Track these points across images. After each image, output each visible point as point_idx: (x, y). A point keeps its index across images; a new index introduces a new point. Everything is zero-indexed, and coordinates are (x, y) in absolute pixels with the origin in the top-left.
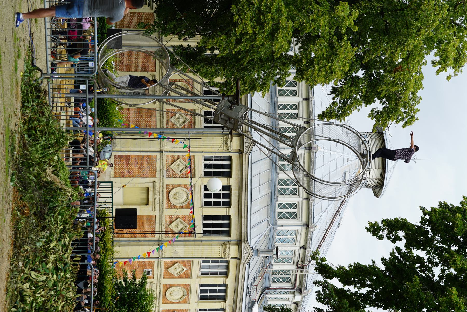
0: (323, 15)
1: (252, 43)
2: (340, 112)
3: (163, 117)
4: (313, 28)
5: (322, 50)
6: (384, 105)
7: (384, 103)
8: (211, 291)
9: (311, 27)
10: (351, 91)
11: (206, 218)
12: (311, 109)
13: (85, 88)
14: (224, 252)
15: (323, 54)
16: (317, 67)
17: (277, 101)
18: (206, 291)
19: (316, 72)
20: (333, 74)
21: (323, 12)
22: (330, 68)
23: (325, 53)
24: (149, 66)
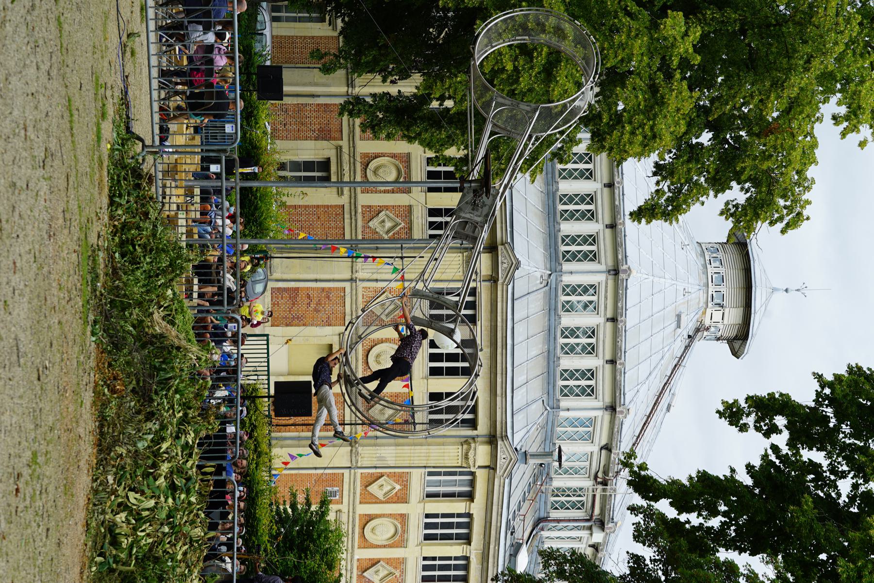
0: (637, 35)
1: (513, 88)
2: (670, 208)
3: (356, 220)
4: (620, 58)
5: (637, 97)
6: (749, 195)
7: (747, 191)
8: (444, 526)
9: (616, 57)
10: (689, 170)
11: (433, 212)
12: (617, 203)
13: (219, 171)
14: (466, 457)
15: (639, 105)
16: (628, 128)
17: (557, 190)
18: (434, 526)
19: (626, 137)
20: (658, 140)
21: (637, 29)
22: (652, 128)
23: (642, 103)
24: (330, 131)
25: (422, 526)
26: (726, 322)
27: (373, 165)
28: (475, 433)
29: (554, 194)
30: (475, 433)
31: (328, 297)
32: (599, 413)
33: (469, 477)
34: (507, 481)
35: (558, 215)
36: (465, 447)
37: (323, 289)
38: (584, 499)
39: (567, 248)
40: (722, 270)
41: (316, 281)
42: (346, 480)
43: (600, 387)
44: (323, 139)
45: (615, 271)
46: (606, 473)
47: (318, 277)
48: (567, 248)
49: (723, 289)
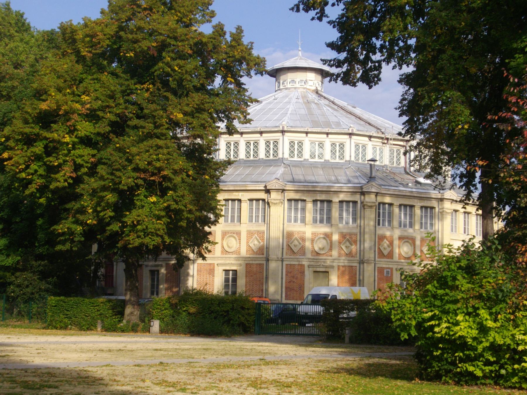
11: (251, 220)
14: (371, 207)
17: (243, 159)
24: (210, 269)
25: (232, 224)
26: (314, 79)
27: (227, 249)
28: (359, 202)
29: (245, 161)
30: (359, 202)
31: (290, 272)
32: (353, 141)
33: (381, 205)
34: (383, 187)
35: (256, 159)
36: (366, 207)
37: (286, 275)
38: (395, 150)
39: (252, 156)
40: (289, 80)
41: (282, 278)
42: (381, 266)
43: (254, 139)
44: (214, 273)
45: (261, 133)
46: (382, 138)
47: (280, 277)
48: (252, 156)
49: (297, 80)
